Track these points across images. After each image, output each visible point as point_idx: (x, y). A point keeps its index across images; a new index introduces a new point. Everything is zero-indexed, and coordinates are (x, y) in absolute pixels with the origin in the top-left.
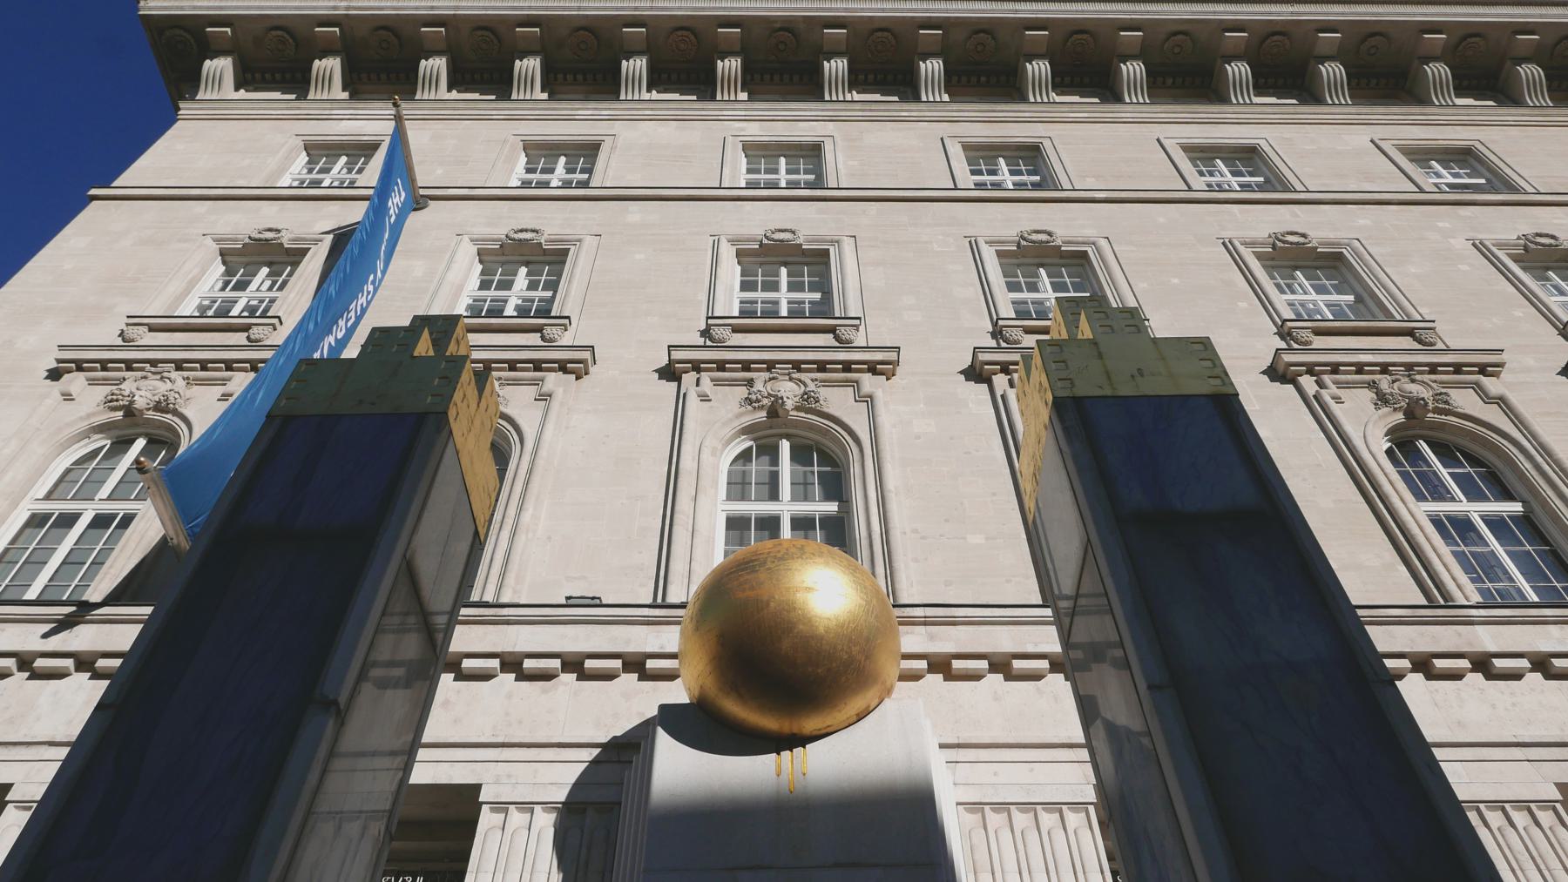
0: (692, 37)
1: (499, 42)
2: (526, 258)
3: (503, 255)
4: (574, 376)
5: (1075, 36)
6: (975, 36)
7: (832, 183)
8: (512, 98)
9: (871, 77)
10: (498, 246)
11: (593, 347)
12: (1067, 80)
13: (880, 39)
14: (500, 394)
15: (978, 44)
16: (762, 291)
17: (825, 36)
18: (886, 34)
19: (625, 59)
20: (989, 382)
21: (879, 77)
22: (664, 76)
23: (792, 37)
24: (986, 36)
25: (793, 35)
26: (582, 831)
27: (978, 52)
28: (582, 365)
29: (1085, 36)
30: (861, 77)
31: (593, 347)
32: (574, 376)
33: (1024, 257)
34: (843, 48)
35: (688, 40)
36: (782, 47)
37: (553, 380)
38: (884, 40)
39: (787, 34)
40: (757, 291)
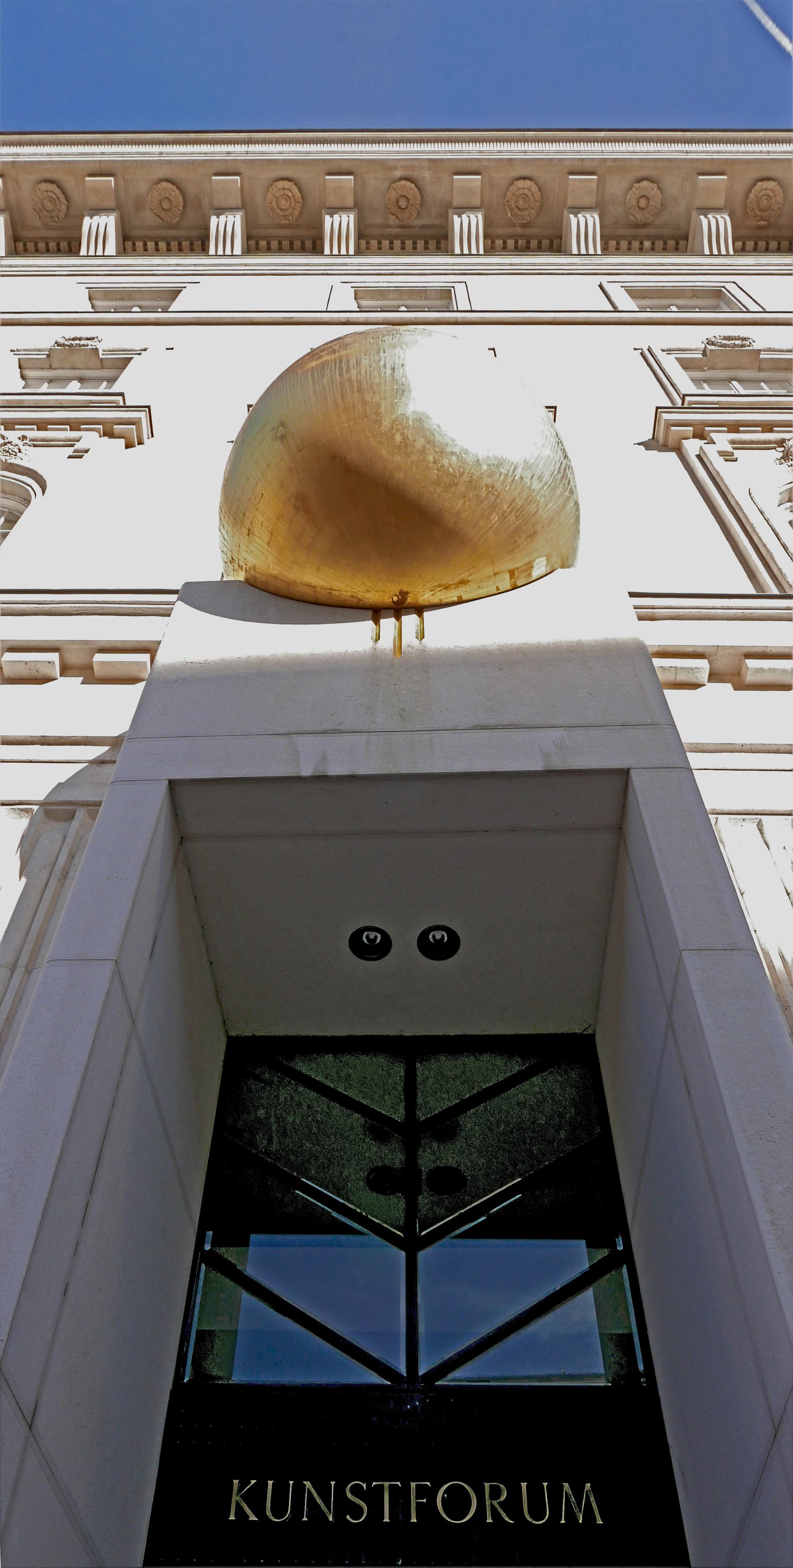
0: (295, 190)
1: (67, 200)
2: (78, 373)
3: (51, 368)
4: (122, 442)
5: (759, 183)
6: (636, 185)
7: (463, 305)
8: (81, 254)
9: (511, 243)
10: (45, 356)
11: (149, 407)
12: (750, 244)
13: (521, 192)
14: (22, 450)
15: (643, 196)
16: (416, 1502)
17: (455, 184)
18: (528, 183)
19: (215, 214)
20: (678, 450)
21: (520, 242)
22: (263, 243)
23: (415, 189)
24: (651, 185)
25: (416, 186)
26: (65, 838)
27: (640, 208)
28: (134, 427)
29: (771, 184)
30: (499, 242)
31: (149, 407)
32: (122, 442)
33: (712, 368)
34: (477, 202)
35: (290, 194)
36: (403, 203)
37: (89, 439)
38: (526, 191)
39: (409, 183)
40: (416, 1499)
